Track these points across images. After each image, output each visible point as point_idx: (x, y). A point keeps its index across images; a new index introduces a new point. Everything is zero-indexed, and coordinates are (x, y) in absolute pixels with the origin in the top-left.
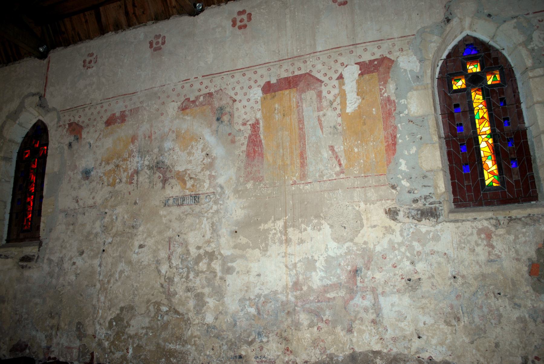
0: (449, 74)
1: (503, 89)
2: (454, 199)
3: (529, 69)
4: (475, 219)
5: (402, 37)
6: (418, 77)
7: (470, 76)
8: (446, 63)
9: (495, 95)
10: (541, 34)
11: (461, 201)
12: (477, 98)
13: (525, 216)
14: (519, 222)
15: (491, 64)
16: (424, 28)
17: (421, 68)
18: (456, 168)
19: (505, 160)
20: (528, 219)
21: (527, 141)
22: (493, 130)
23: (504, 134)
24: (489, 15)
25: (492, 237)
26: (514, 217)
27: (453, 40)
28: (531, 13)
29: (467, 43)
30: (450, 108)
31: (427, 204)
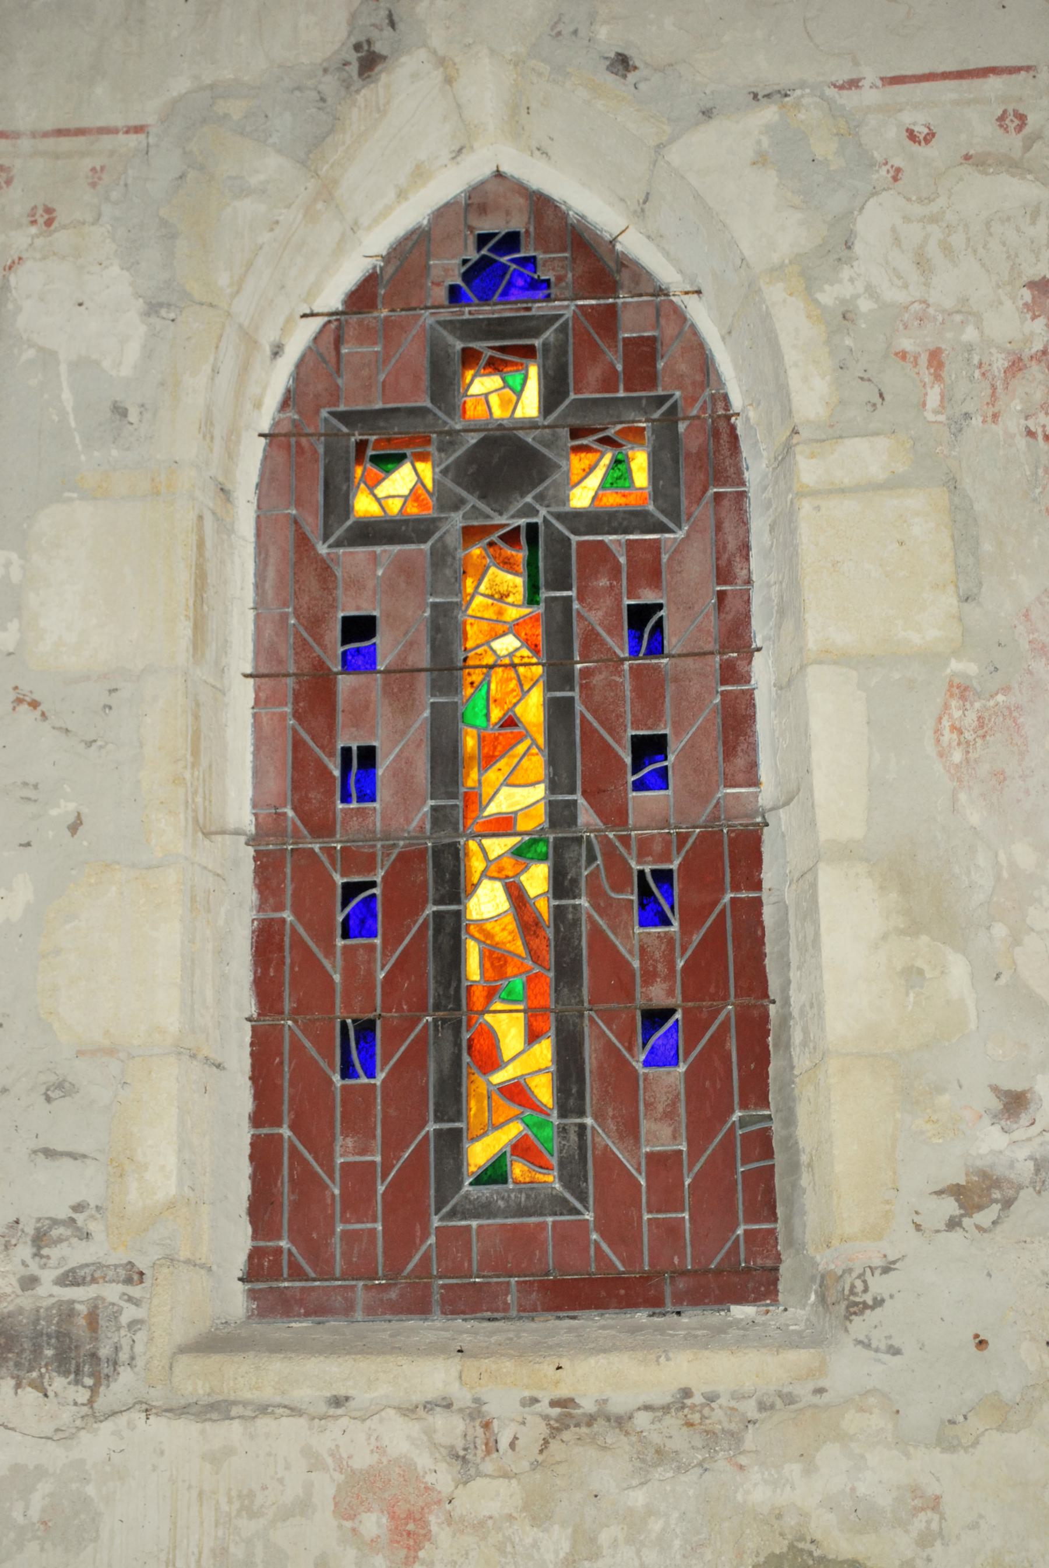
0: (344, 417)
1: (655, 547)
2: (255, 1255)
3: (805, 433)
4: (338, 1402)
5: (60, 133)
6: (120, 411)
7: (473, 439)
8: (338, 342)
9: (603, 582)
10: (907, 219)
11: (297, 1273)
12: (496, 597)
13: (659, 1400)
14: (612, 1437)
15: (609, 382)
16: (216, 91)
17: (148, 354)
18: (297, 1047)
19: (609, 1018)
20: (672, 1422)
21: (758, 903)
22: (560, 814)
23: (625, 840)
24: (622, 63)
25: (428, 1536)
26: (587, 1405)
27: (402, 195)
28: (870, 75)
29: (486, 226)
30: (319, 639)
31: (47, 1276)
